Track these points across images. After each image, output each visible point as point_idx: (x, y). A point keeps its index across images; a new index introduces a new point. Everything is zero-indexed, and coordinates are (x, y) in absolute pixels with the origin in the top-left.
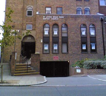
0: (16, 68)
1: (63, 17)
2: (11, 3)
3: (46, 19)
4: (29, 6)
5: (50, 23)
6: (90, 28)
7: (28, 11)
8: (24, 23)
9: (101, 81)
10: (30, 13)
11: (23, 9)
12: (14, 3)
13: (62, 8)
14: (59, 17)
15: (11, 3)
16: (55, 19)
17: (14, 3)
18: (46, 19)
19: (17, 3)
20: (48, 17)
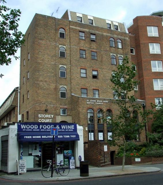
0: (87, 162)
1: (107, 102)
2: (42, 81)
3: (90, 103)
4: (62, 86)
5: (95, 108)
6: (88, 113)
7: (61, 93)
8: (58, 107)
9: (84, 179)
10: (63, 95)
11: (56, 89)
12: (46, 81)
13: (98, 90)
14: (104, 101)
15: (42, 81)
16: (100, 103)
17: (46, 81)
18: (90, 103)
19: (48, 81)
20: (92, 101)
